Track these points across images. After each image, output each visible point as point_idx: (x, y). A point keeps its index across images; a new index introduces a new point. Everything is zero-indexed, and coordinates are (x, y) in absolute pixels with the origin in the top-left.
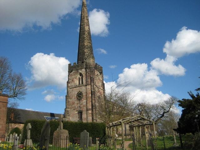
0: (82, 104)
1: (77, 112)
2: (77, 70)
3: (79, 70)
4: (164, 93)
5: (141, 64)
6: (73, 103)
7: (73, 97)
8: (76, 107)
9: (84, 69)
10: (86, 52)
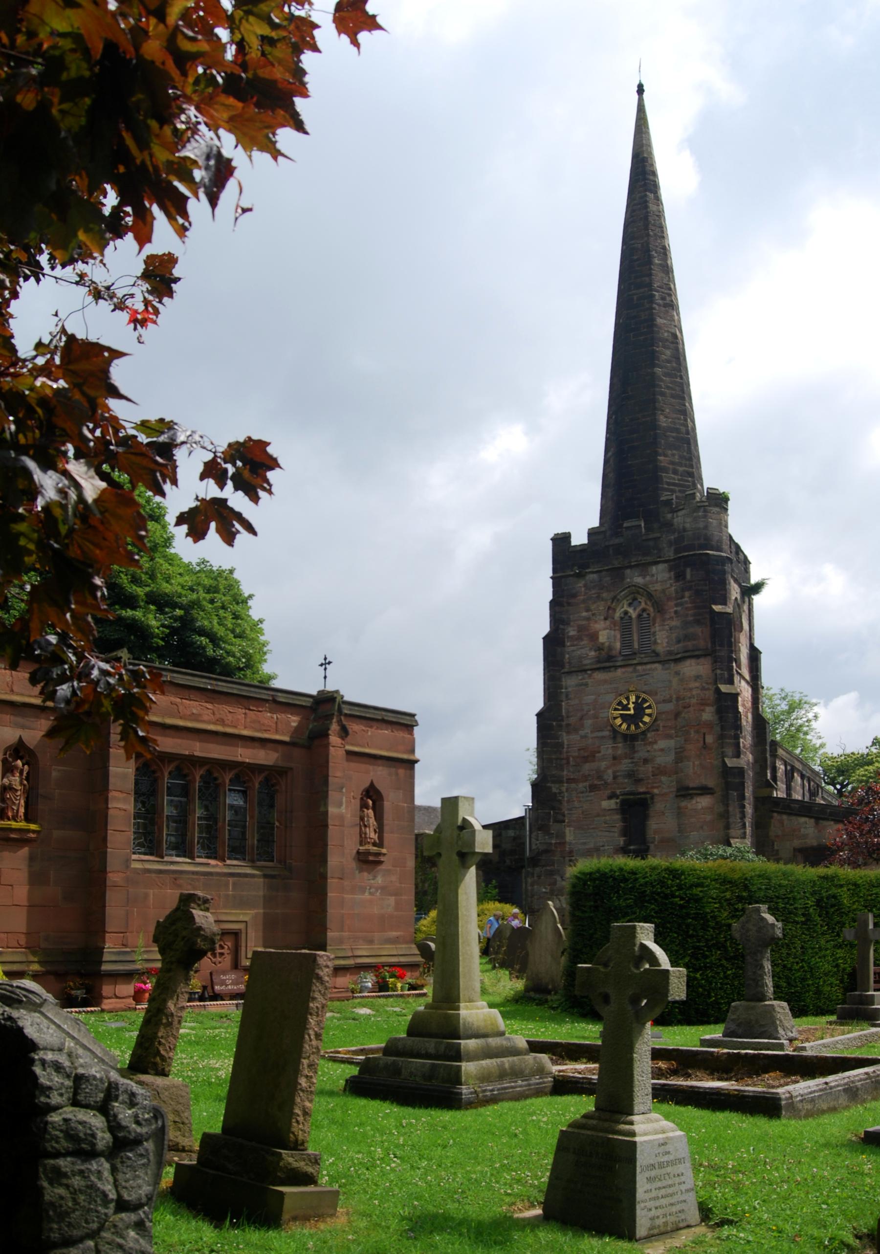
0: (646, 761)
1: (612, 804)
2: (617, 574)
3: (628, 571)
4: (226, 484)
5: (235, 168)
6: (590, 756)
7: (588, 723)
8: (609, 776)
9: (661, 567)
10: (665, 470)
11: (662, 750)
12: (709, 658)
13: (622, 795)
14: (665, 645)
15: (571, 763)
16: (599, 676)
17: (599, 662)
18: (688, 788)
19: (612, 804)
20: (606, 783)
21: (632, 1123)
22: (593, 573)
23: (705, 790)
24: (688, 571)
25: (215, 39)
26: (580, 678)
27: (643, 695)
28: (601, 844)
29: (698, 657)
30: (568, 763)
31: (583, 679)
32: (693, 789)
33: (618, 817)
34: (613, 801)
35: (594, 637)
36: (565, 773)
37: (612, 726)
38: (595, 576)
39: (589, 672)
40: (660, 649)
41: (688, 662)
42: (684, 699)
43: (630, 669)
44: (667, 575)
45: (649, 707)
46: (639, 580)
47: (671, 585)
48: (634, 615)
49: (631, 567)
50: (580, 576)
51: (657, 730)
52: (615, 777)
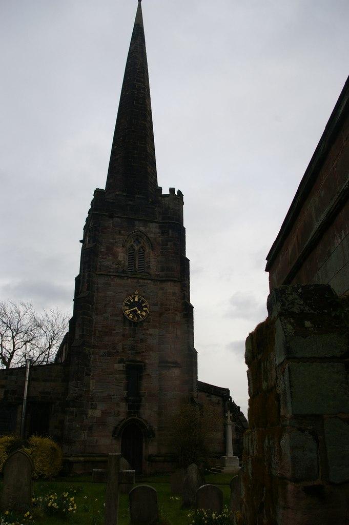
0: (142, 341)
1: (120, 367)
8: (120, 347)
11: (151, 335)
12: (179, 283)
13: (128, 361)
14: (155, 270)
15: (97, 335)
16: (117, 280)
17: (117, 272)
18: (167, 362)
19: (120, 367)
20: (117, 352)
21: (223, 469)
22: (118, 217)
23: (176, 365)
24: (170, 231)
25: (136, 26)
26: (106, 279)
27: (142, 299)
28: (112, 394)
29: (175, 281)
30: (95, 334)
31: (108, 280)
32: (169, 363)
33: (124, 376)
34: (121, 365)
35: (115, 256)
36: (92, 341)
37: (123, 314)
38: (119, 220)
39: (112, 277)
40: (151, 272)
41: (169, 283)
42: (166, 305)
43: (136, 280)
44: (158, 230)
45: (146, 306)
46: (142, 229)
47: (159, 237)
48: (137, 249)
49: (139, 220)
50: (111, 216)
51: (149, 322)
52: (123, 349)
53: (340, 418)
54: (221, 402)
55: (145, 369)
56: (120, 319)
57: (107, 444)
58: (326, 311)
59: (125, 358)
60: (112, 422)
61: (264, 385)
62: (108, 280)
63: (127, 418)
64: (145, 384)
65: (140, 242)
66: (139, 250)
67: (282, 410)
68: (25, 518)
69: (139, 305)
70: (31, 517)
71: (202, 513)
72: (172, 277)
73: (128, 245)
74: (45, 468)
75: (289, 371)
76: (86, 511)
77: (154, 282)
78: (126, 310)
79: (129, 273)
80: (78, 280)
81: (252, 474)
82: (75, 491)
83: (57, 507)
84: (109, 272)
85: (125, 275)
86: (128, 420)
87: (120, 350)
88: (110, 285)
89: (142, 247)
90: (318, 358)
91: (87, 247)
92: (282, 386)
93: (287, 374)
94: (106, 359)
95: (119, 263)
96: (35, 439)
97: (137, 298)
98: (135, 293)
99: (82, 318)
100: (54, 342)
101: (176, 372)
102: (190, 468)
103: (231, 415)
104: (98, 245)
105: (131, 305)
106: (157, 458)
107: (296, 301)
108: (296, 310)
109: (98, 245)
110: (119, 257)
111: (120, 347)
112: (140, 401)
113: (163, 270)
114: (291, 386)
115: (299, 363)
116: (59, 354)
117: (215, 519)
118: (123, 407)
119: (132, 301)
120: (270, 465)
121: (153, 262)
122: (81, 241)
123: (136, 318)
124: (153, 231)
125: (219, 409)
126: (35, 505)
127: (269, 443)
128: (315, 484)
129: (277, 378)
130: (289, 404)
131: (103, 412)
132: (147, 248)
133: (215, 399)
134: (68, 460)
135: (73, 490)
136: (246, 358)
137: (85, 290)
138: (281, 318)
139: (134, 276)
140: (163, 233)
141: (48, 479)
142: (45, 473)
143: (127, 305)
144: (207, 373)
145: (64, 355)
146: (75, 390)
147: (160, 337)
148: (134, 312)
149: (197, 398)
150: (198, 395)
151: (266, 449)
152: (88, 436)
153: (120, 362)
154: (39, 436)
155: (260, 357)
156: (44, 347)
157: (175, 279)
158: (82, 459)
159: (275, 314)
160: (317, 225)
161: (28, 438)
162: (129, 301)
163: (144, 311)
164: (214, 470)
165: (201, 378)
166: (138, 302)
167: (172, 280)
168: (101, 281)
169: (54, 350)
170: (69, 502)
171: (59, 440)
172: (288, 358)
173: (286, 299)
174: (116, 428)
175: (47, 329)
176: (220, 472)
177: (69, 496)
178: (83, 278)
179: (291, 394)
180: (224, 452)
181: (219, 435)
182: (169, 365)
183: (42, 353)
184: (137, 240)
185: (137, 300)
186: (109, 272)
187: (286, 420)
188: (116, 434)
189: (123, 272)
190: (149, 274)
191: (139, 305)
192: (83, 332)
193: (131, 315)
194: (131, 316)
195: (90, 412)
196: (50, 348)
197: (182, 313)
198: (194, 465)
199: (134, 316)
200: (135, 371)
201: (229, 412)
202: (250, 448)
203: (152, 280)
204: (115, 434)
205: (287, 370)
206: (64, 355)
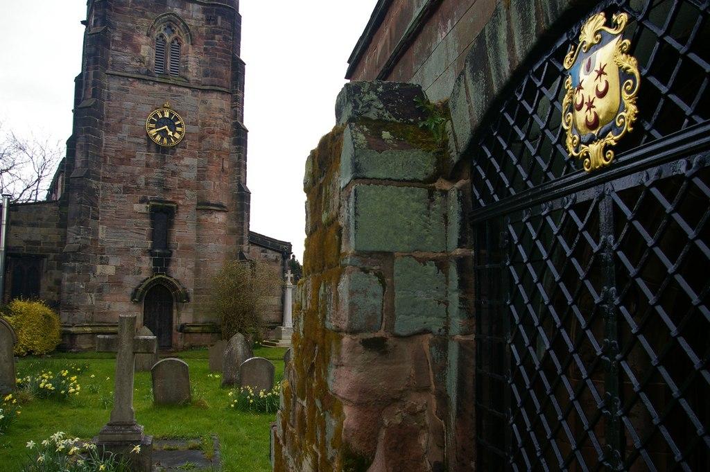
0: (174, 173)
1: (142, 208)
8: (141, 181)
11: (187, 166)
13: (153, 201)
16: (140, 86)
17: (138, 73)
18: (208, 204)
19: (142, 208)
20: (138, 187)
23: (221, 208)
24: (219, 18)
27: (175, 114)
30: (105, 161)
31: (124, 84)
32: (213, 205)
33: (148, 221)
34: (144, 205)
35: (136, 49)
36: (101, 171)
39: (130, 80)
40: (189, 76)
41: (215, 95)
43: (166, 87)
44: (201, 16)
45: (180, 125)
46: (178, 11)
48: (168, 40)
51: (185, 148)
52: (147, 184)
53: (414, 257)
54: (280, 260)
55: (177, 212)
56: (142, 141)
57: (123, 308)
58: (412, 120)
59: (149, 197)
60: (131, 282)
61: (324, 217)
62: (124, 84)
63: (151, 277)
64: (177, 232)
65: (173, 31)
66: (173, 42)
67: (343, 247)
68: (7, 402)
69: (171, 123)
70: (14, 401)
71: (247, 390)
72: (218, 86)
73: (156, 34)
74: (35, 342)
75: (355, 195)
76: (94, 392)
77: (193, 91)
78: (152, 128)
79: (157, 75)
80: (79, 81)
81: (303, 333)
82: (79, 369)
83: (53, 388)
84: (127, 72)
85: (151, 78)
86: (153, 279)
87: (142, 185)
88: (127, 91)
89: (176, 39)
90: (395, 180)
91: (93, 31)
92: (346, 215)
93: (352, 199)
94: (121, 197)
95: (141, 61)
96: (19, 304)
97: (168, 113)
98: (165, 105)
99: (86, 137)
100: (45, 172)
101: (220, 218)
102: (234, 338)
103: (292, 275)
104: (109, 29)
105: (159, 123)
106: (192, 328)
107: (374, 104)
108: (372, 115)
109: (109, 29)
110: (142, 51)
111: (141, 181)
112: (170, 254)
113: (206, 75)
114: (356, 214)
115: (369, 185)
116: (53, 189)
117: (263, 398)
118: (147, 263)
119: (160, 116)
120: (324, 317)
121: (193, 62)
122: (83, 22)
123: (165, 140)
124: (194, 16)
125: (277, 268)
126: (21, 386)
127: (325, 290)
128: (376, 336)
129: (340, 206)
130: (352, 238)
131: (117, 268)
132: (183, 40)
133: (272, 255)
134: (70, 331)
135: (76, 367)
136: (305, 184)
137: (90, 96)
138: (350, 126)
139: (163, 80)
140: (208, 20)
141: (40, 356)
142: (36, 348)
143: (152, 121)
144: (262, 222)
145: (59, 189)
146: (77, 238)
147: (200, 169)
148: (164, 133)
149: (248, 252)
150: (249, 248)
151: (321, 297)
152: (96, 299)
153: (142, 202)
154: (25, 301)
155: (321, 181)
156: (31, 180)
157: (223, 89)
158: (88, 329)
159: (344, 119)
160: (416, 13)
161: (9, 302)
162: (156, 116)
163: (178, 132)
164: (266, 343)
165: (251, 229)
166: (169, 119)
167: (219, 91)
168: (114, 84)
169: (46, 184)
170: (69, 382)
171: (55, 305)
172: (355, 178)
173: (360, 99)
174: (136, 290)
175: (33, 153)
176: (275, 345)
177: (69, 375)
178: (87, 78)
179: (355, 224)
180: (281, 322)
181: (275, 301)
182: (211, 208)
183: (28, 188)
184: (169, 27)
185: (167, 115)
186: (127, 72)
187: (346, 258)
188: (136, 297)
189: (148, 73)
190: (185, 79)
191: (171, 123)
192: (88, 156)
193: (158, 136)
194: (158, 138)
195: (99, 268)
196: (38, 180)
197: (232, 138)
198: (240, 335)
199: (162, 138)
200: (162, 216)
201: (289, 271)
202: (303, 300)
203: (190, 88)
204: (135, 297)
205: (352, 194)
206: (59, 189)
